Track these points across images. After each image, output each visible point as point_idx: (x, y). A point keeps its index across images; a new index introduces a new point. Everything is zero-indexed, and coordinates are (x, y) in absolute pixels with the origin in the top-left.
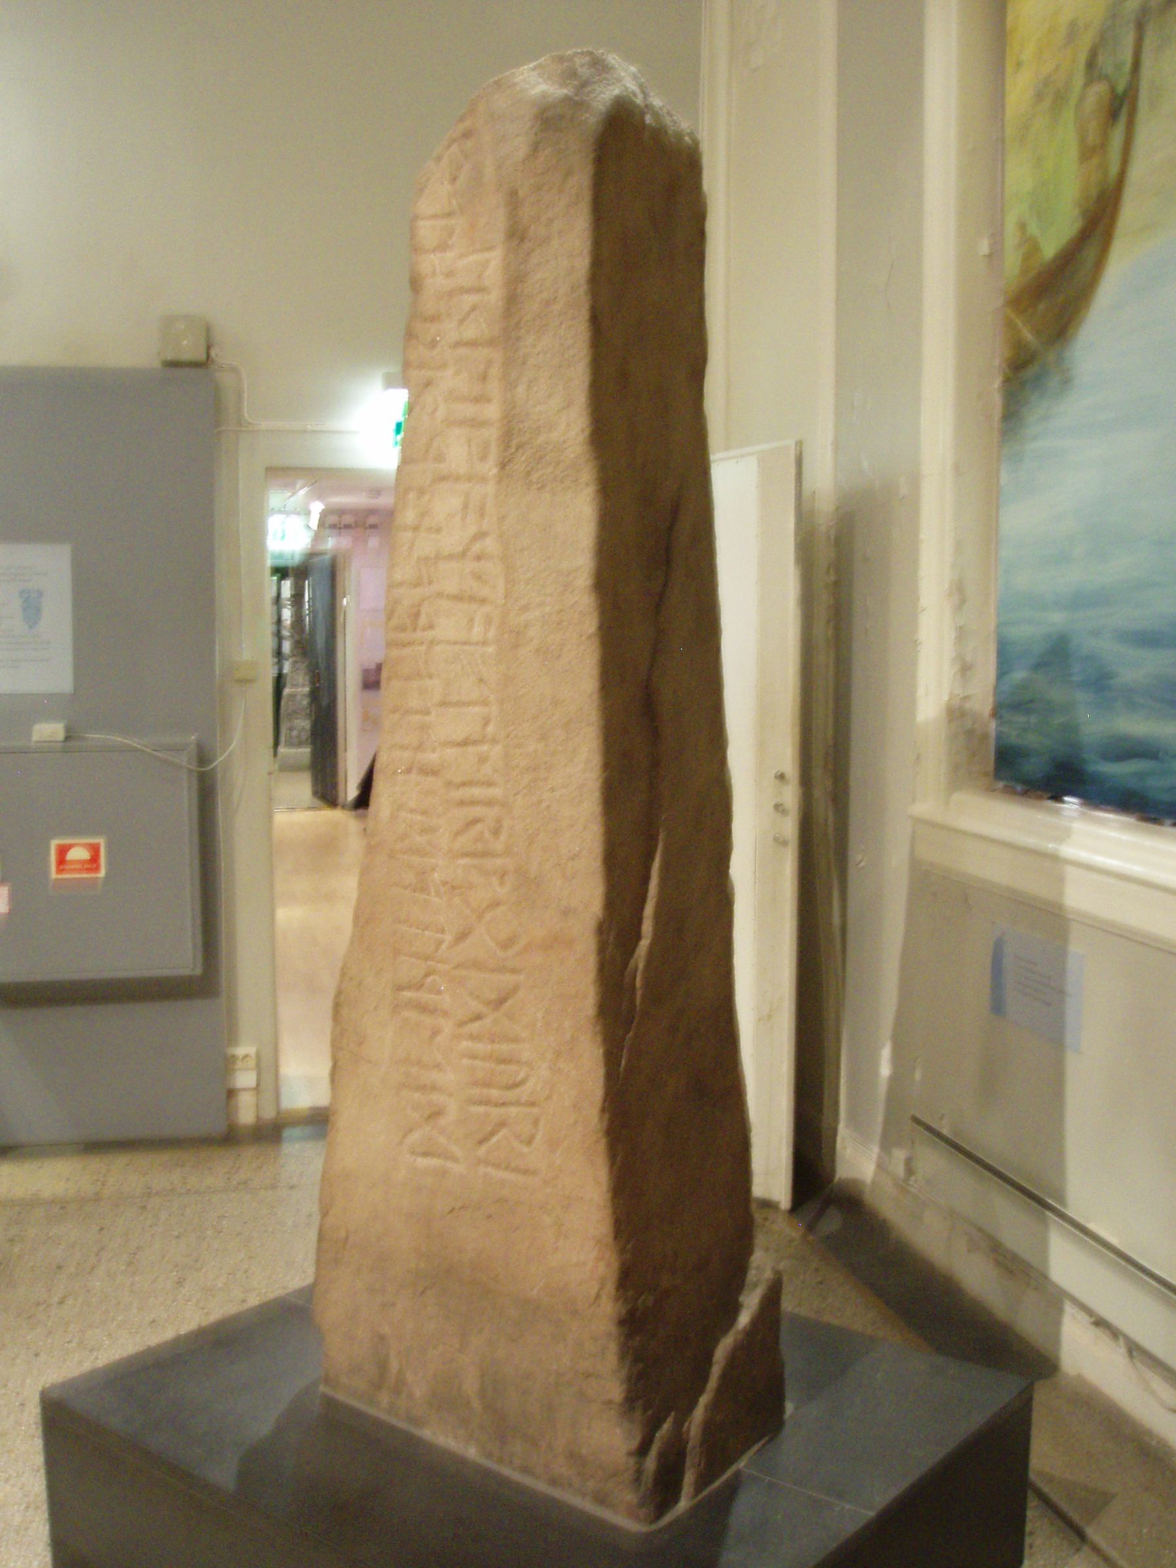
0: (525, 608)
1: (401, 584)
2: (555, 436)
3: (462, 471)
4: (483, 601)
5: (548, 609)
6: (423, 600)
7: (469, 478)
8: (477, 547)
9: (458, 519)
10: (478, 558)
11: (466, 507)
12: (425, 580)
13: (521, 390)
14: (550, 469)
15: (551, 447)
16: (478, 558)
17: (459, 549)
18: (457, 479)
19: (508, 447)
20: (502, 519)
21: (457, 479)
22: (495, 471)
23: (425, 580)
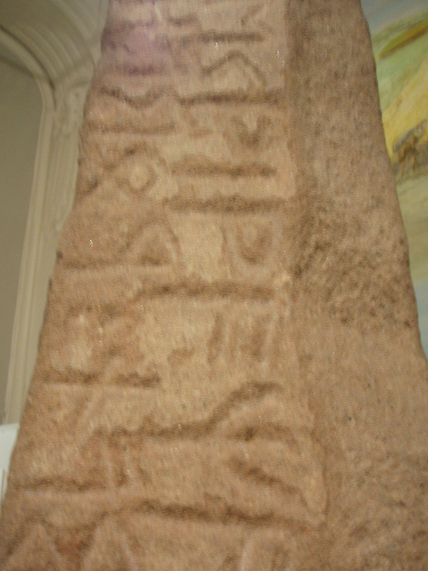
0: (360, 532)
1: (43, 483)
2: (364, 242)
3: (209, 278)
4: (265, 519)
5: (397, 531)
6: (104, 515)
7: (225, 290)
8: (243, 414)
9: (200, 359)
10: (249, 434)
11: (216, 337)
12: (110, 475)
13: (318, 166)
14: (356, 293)
15: (357, 259)
16: (249, 434)
17: (203, 416)
18: (196, 290)
19: (304, 244)
20: (305, 359)
21: (196, 290)
22: (286, 277)
23: (110, 475)
